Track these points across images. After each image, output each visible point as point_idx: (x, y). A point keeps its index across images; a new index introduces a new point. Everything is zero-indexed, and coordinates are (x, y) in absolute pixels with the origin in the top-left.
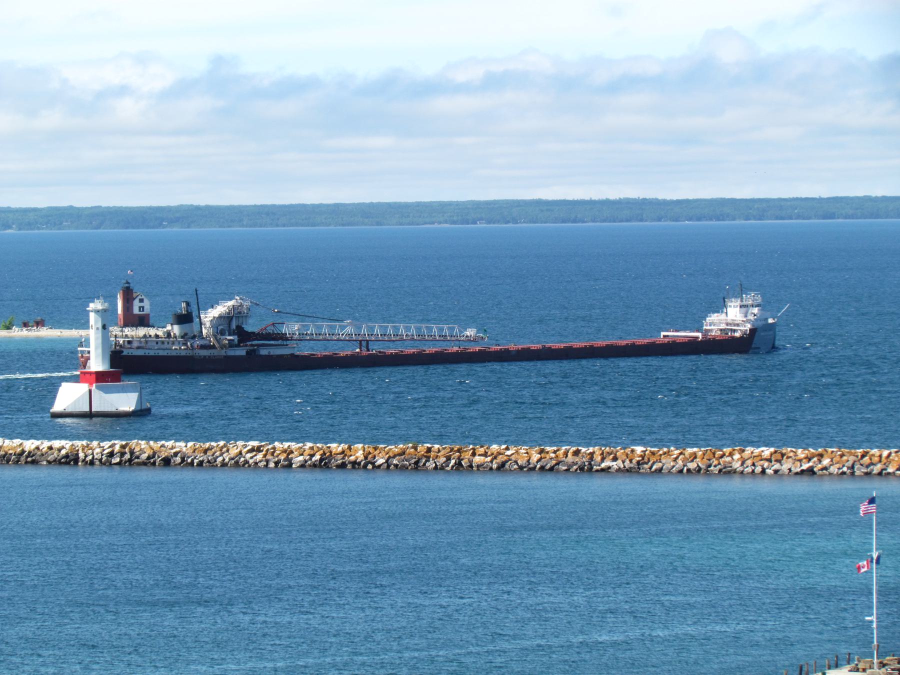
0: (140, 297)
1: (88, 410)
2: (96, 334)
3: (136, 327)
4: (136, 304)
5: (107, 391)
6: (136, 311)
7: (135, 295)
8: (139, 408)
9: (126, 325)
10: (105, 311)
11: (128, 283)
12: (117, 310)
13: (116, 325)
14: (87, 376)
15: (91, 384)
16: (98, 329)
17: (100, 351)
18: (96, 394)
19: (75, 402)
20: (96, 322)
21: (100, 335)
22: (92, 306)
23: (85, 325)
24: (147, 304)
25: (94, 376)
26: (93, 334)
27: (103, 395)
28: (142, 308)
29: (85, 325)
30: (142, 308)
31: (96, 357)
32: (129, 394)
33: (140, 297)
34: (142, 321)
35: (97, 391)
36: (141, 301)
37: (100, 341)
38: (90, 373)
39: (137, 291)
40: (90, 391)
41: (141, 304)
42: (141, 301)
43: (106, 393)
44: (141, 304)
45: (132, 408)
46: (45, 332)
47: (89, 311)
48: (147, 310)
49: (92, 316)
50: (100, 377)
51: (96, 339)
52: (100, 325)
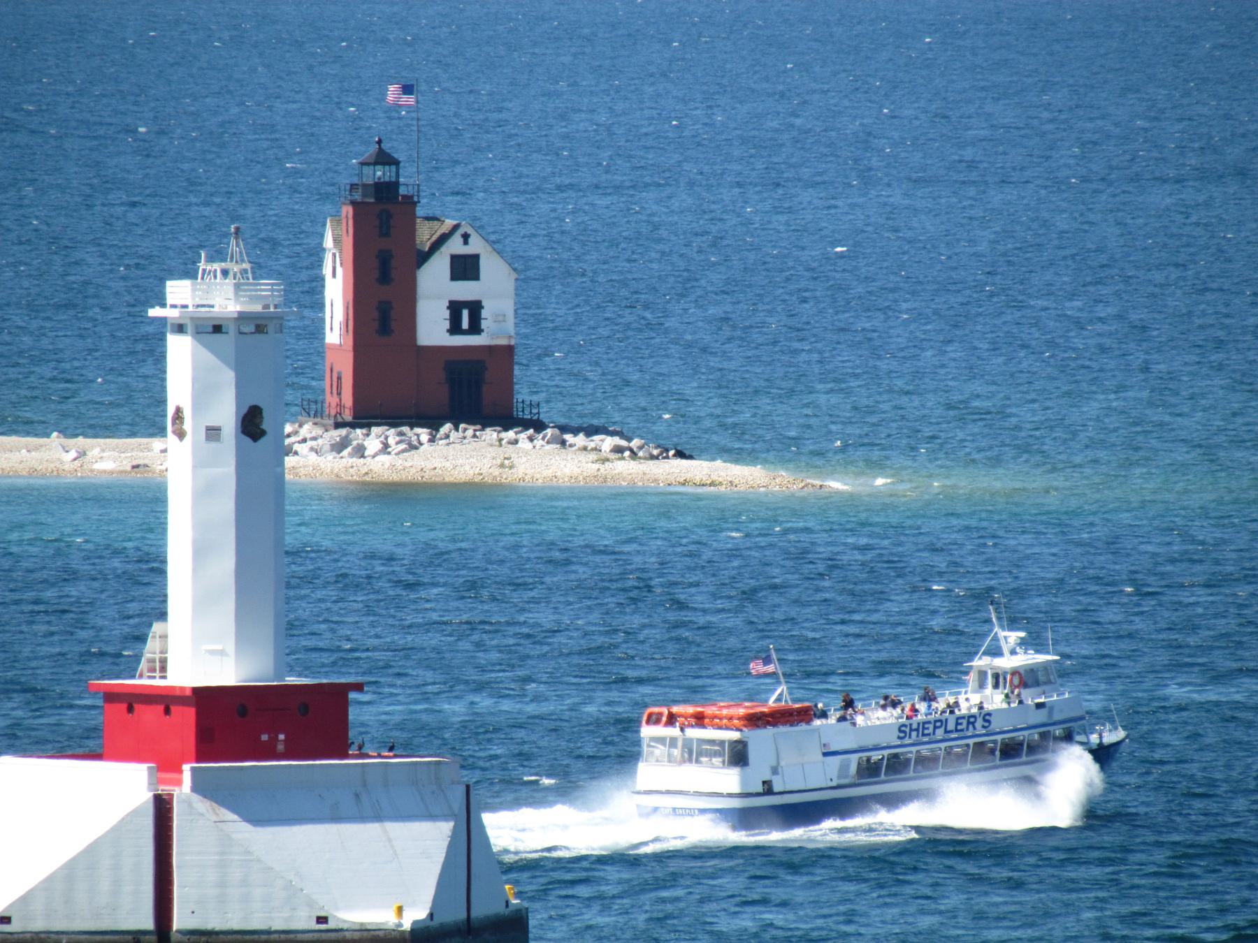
0: (455, 246)
1: (145, 920)
2: (199, 464)
3: (433, 423)
4: (435, 288)
5: (263, 810)
6: (432, 328)
7: (425, 235)
8: (290, 493)
9: (367, 413)
10: (256, 325)
11: (384, 158)
12: (316, 331)
13: (313, 410)
14: (149, 715)
15: (167, 766)
16: (213, 433)
17: (225, 564)
18: (198, 821)
19: (70, 871)
20: (202, 393)
21: (227, 470)
22: (179, 292)
23: (145, 414)
24: (496, 288)
25: (187, 716)
26: (187, 473)
27: (242, 830)
28: (465, 315)
29: (145, 414)
30: (465, 315)
31: (202, 602)
32: (398, 830)
33: (455, 246)
34: (472, 391)
35: (202, 805)
36: (465, 268)
37: (226, 506)
38: (167, 700)
39: (436, 214)
40: (162, 809)
41: (465, 290)
42: (465, 268)
43: (257, 819)
44: (465, 290)
45: (415, 914)
46: (698, 470)
47: (159, 330)
48: (499, 326)
49: (181, 353)
50: (228, 726)
51: (202, 494)
52: (226, 415)
